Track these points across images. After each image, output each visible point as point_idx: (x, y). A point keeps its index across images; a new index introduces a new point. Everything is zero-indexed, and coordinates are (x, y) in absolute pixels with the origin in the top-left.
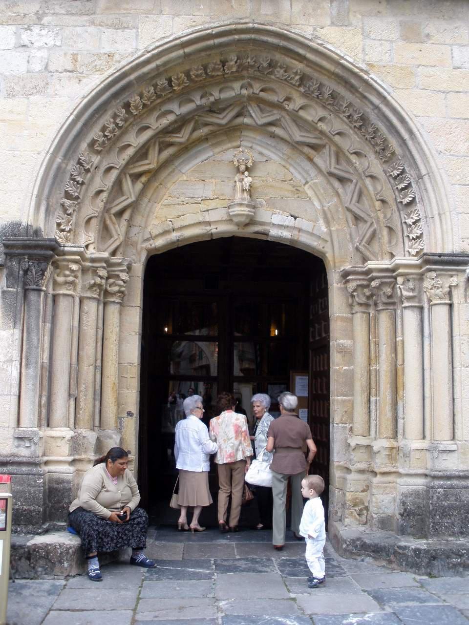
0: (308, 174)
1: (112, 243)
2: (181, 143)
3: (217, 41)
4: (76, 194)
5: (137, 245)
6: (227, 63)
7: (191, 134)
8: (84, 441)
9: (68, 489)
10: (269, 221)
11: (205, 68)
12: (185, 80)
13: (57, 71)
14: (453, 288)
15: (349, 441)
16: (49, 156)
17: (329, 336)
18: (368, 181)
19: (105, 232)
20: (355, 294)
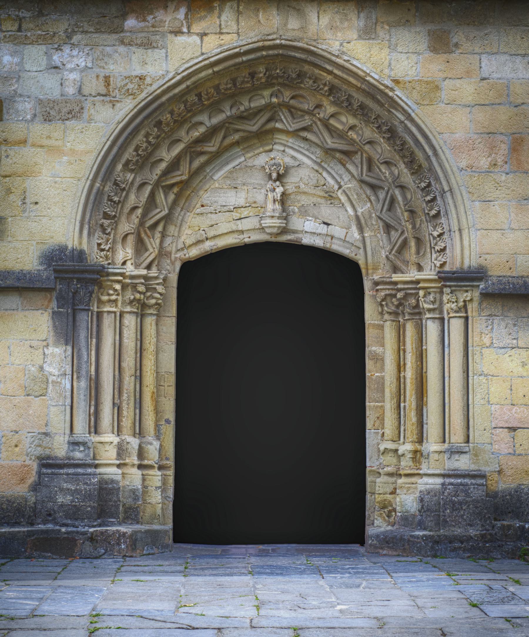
0: (341, 178)
2: (211, 152)
4: (114, 213)
7: (222, 142)
8: (128, 446)
10: (302, 229)
13: (91, 95)
14: (467, 303)
16: (89, 182)
20: (384, 303)
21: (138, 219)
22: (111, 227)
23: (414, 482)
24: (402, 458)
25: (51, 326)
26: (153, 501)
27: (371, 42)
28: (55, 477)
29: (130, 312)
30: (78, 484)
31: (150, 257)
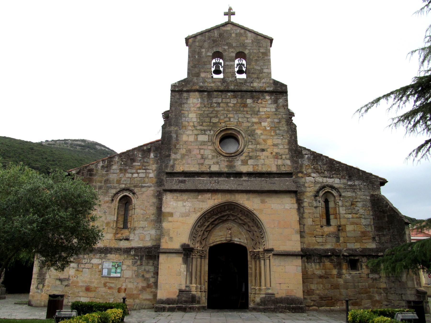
18: (255, 232)
19: (201, 243)
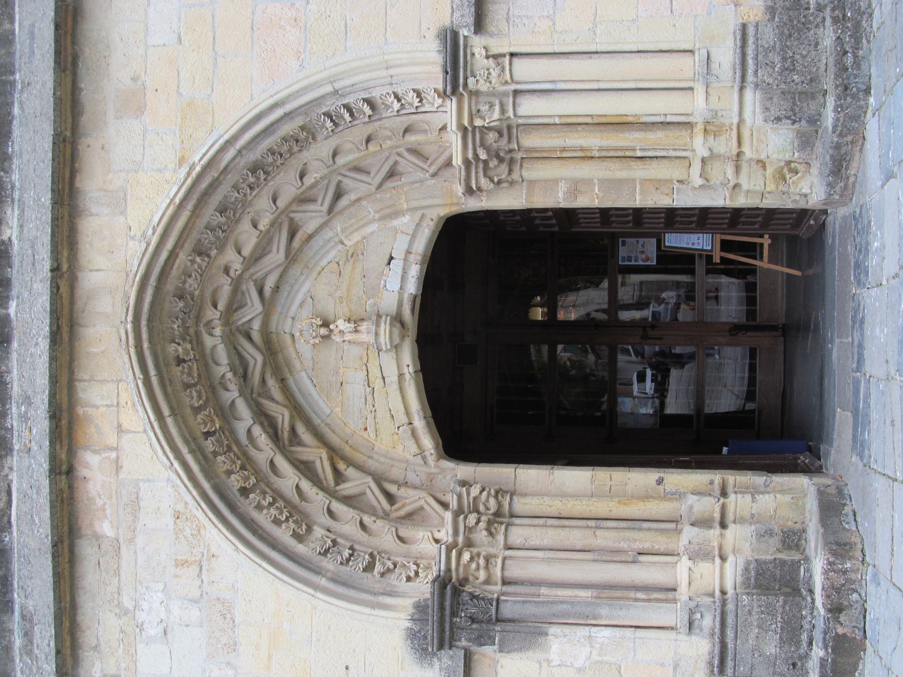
0: (329, 241)
1: (431, 506)
2: (292, 417)
3: (152, 372)
4: (367, 557)
5: (431, 474)
6: (181, 356)
7: (278, 403)
9: (757, 563)
11: (187, 386)
12: (206, 413)
14: (490, 53)
15: (697, 186)
16: (319, 595)
17: (552, 209)
18: (341, 160)
20: (496, 180)
21: (377, 521)
22: (386, 561)
23: (750, 133)
24: (715, 151)
25: (520, 655)
26: (771, 506)
27: (129, 197)
28: (738, 656)
29: (506, 536)
30: (751, 624)
31: (432, 504)
